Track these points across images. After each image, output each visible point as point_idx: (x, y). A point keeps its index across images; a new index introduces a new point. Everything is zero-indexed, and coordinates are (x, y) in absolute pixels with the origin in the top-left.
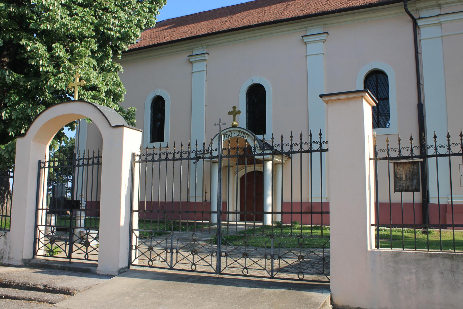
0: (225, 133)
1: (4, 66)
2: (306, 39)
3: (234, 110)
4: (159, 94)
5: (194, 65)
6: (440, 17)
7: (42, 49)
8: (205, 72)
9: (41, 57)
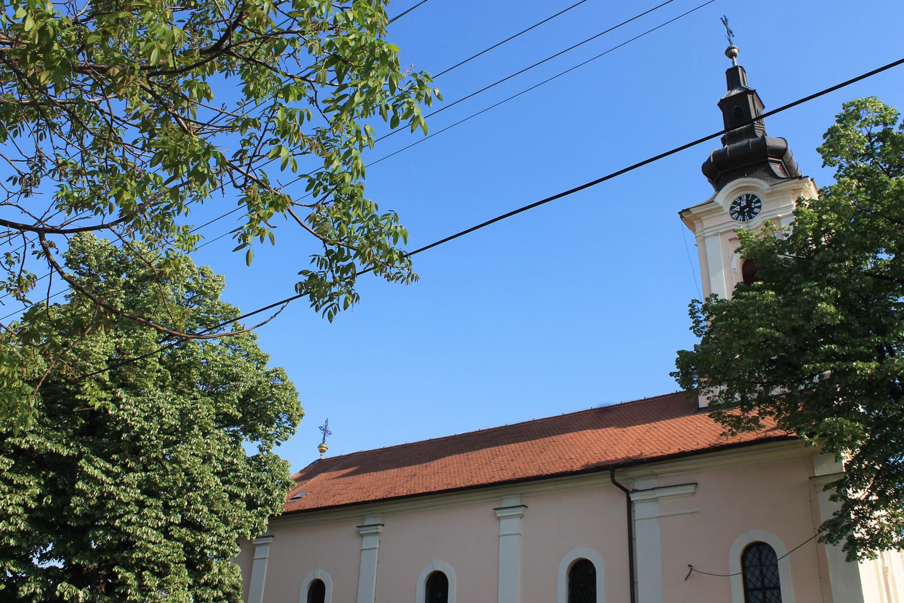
1: (100, 579)
2: (500, 514)
5: (365, 539)
6: (655, 491)
7: (131, 577)
8: (377, 550)
9: (129, 586)
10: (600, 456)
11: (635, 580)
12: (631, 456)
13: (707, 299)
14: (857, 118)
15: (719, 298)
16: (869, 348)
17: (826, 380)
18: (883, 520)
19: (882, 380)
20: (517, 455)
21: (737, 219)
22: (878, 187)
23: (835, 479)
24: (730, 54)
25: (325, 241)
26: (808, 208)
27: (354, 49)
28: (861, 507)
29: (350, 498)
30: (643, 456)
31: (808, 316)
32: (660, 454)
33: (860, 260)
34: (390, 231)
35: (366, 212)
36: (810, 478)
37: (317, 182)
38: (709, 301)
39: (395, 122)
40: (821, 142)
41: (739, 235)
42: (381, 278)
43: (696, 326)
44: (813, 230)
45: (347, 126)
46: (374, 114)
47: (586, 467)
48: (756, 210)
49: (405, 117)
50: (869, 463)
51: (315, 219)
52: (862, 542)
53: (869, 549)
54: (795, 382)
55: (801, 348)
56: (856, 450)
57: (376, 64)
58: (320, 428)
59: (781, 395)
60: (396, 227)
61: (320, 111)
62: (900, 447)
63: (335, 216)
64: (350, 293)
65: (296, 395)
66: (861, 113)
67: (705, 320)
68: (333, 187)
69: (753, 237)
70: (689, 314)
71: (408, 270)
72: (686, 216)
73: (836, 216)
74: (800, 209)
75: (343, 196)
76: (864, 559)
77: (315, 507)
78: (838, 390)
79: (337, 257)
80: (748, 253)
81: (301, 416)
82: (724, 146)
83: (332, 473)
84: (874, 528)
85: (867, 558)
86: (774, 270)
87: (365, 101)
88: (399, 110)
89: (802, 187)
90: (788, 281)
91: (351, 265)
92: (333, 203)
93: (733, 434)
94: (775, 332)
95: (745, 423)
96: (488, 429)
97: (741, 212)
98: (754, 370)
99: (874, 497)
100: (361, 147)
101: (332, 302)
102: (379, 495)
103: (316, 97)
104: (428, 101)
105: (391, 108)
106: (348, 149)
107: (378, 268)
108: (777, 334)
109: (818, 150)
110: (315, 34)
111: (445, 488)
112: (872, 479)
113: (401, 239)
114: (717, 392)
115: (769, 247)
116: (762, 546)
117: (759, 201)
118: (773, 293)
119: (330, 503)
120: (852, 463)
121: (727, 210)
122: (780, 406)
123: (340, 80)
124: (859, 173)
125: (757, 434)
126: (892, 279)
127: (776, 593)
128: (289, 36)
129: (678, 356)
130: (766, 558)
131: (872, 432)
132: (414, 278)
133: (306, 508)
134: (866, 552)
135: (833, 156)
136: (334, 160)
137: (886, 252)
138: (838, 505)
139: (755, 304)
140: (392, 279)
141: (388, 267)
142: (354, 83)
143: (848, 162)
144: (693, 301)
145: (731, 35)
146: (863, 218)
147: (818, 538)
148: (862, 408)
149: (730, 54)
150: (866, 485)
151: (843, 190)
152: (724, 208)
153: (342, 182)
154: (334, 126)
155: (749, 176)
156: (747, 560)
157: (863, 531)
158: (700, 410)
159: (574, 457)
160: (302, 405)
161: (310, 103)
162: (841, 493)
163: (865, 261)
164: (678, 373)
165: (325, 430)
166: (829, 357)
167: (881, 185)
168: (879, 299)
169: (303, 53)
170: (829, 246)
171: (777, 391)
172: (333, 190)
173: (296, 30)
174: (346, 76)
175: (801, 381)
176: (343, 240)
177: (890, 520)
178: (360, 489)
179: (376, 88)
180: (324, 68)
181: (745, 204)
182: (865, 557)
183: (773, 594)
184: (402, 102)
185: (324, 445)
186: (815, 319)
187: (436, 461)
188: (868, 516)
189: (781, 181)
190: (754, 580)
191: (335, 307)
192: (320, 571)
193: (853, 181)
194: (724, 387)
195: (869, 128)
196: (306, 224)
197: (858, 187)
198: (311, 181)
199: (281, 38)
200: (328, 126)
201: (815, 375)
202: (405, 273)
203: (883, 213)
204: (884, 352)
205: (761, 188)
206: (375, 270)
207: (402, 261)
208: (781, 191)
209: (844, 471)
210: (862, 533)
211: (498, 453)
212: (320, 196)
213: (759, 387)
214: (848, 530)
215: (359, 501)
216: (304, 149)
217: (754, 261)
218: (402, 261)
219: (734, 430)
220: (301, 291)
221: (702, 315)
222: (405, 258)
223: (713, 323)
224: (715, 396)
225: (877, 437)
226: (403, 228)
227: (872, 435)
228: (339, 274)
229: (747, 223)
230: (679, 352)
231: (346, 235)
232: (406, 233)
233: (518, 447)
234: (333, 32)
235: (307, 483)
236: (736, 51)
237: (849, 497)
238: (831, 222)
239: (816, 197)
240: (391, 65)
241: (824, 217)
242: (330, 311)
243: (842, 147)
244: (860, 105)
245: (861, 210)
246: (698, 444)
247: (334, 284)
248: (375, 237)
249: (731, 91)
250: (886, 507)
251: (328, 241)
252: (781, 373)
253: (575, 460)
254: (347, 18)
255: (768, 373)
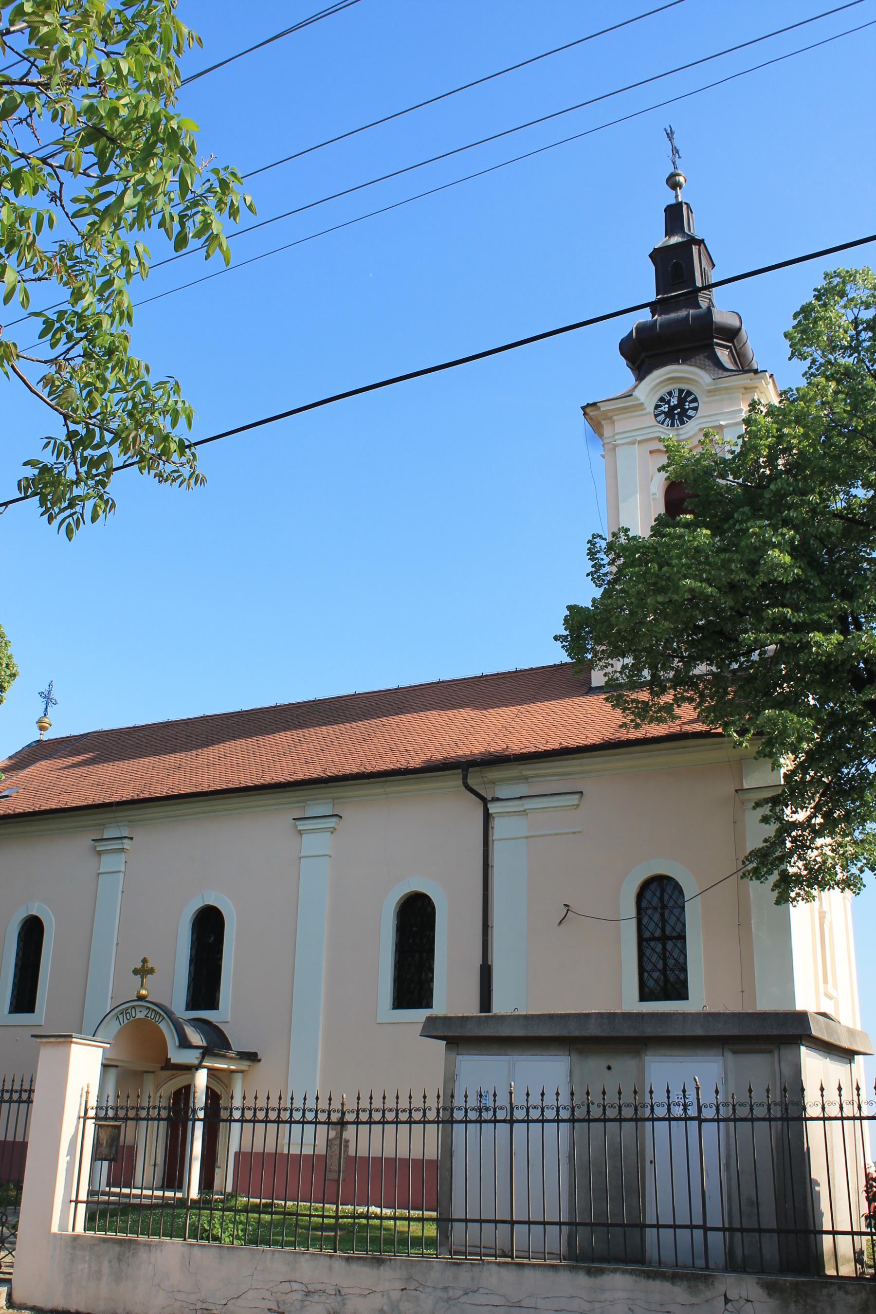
0: (123, 1009)
2: (302, 826)
3: (143, 966)
4: (34, 913)
5: (105, 858)
6: (524, 801)
8: (122, 875)
10: (449, 749)
11: (489, 924)
12: (492, 750)
13: (614, 535)
14: (842, 294)
15: (631, 534)
16: (830, 617)
17: (768, 658)
18: (827, 851)
19: (843, 663)
20: (329, 743)
21: (662, 423)
22: (860, 395)
23: (769, 794)
24: (673, 183)
25: (66, 417)
26: (764, 417)
27: (126, 121)
28: (800, 832)
29: (83, 798)
30: (510, 752)
31: (752, 567)
32: (533, 749)
33: (828, 495)
34: (167, 408)
35: (131, 376)
36: (736, 791)
37: (57, 325)
38: (617, 538)
39: (181, 242)
40: (790, 324)
41: (665, 446)
42: (148, 478)
43: (596, 572)
44: (769, 447)
45: (108, 242)
46: (149, 226)
47: (429, 763)
48: (690, 413)
49: (198, 235)
50: (815, 774)
51: (53, 382)
52: (798, 880)
53: (806, 888)
54: (727, 658)
55: (738, 612)
56: (800, 755)
57: (159, 148)
58: (41, 694)
59: (707, 675)
60: (176, 402)
61: (67, 214)
62: (857, 753)
63: (85, 379)
64: (101, 497)
65: (6, 644)
66: (848, 287)
67: (609, 564)
68: (82, 334)
69: (685, 452)
70: (588, 554)
71: (191, 467)
72: (591, 414)
73: (802, 430)
74: (754, 416)
75: (97, 350)
76: (798, 901)
77: (31, 810)
78: (784, 673)
79: (84, 443)
80: (676, 472)
81: (13, 675)
82: (653, 317)
83: (58, 761)
84: (815, 860)
85: (803, 899)
86: (710, 499)
87: (140, 205)
88: (189, 224)
89: (757, 385)
90: (729, 516)
91: (105, 457)
92: (81, 359)
93: (637, 726)
94: (707, 586)
95: (654, 712)
96: (290, 704)
97: (670, 414)
98: (673, 639)
99: (819, 820)
100: (129, 275)
101: (74, 510)
102: (127, 794)
103: (60, 192)
104: (234, 212)
105: (176, 219)
106: (107, 277)
107: (144, 461)
108: (710, 590)
109: (786, 335)
110: (67, 90)
111: (224, 787)
112: (818, 795)
113: (182, 420)
114: (618, 665)
115: (707, 467)
116: (665, 882)
117: (695, 400)
118: (709, 532)
119: (53, 805)
120: (793, 772)
121: (650, 408)
122: (703, 690)
123: (102, 169)
124: (837, 372)
125: (670, 727)
126: (867, 525)
127: (679, 944)
128: (25, 90)
129: (568, 613)
130: (670, 897)
131: (823, 732)
132: (199, 480)
133: (17, 812)
134: (802, 893)
135: (805, 345)
136: (86, 293)
137: (863, 486)
138: (771, 830)
139: (682, 546)
140: (166, 480)
141: (161, 462)
142: (124, 174)
143: (823, 356)
144: (594, 536)
145: (677, 155)
146: (838, 436)
147: (740, 873)
148: (813, 698)
149: (673, 183)
150: (810, 803)
151: (816, 395)
152: (646, 405)
153: (96, 328)
154: (86, 240)
155: (684, 362)
156: (644, 900)
157: (800, 864)
158: (591, 690)
159: (411, 749)
160: (15, 660)
161: (52, 200)
162: (775, 813)
163: (834, 497)
164: (566, 637)
165: (48, 698)
166: (779, 625)
167: (865, 393)
168: (848, 551)
169: (43, 121)
170: (788, 472)
171: (701, 669)
172: (82, 339)
173: (36, 81)
174: (112, 164)
175: (734, 657)
176: (95, 417)
177: (835, 850)
178: (98, 785)
179: (158, 186)
180: (79, 147)
181: (676, 403)
182: (800, 899)
183: (675, 945)
184: (194, 210)
185: (46, 720)
186: (762, 572)
187: (211, 748)
188: (808, 844)
189: (729, 373)
190: (652, 926)
191: (78, 517)
192: (37, 904)
193: (830, 383)
194: (629, 660)
195: (856, 311)
196: (39, 389)
197: (836, 393)
198: (49, 324)
199: (12, 92)
200: (79, 240)
201: (754, 650)
202: (186, 471)
203: (864, 433)
204: (849, 624)
205: (700, 381)
206: (140, 465)
207: (182, 454)
208: (726, 389)
209: (782, 783)
210: (798, 867)
211: (303, 739)
212: (61, 348)
213: (676, 663)
214: (782, 862)
215: (97, 803)
216: (40, 273)
217: (684, 485)
218: (182, 454)
219: (638, 721)
220: (26, 491)
221: (604, 557)
222: (187, 450)
223: (620, 570)
224: (616, 672)
225: (829, 739)
226: (187, 405)
227: (822, 737)
228: (85, 468)
229: (676, 429)
230: (569, 608)
231: (98, 410)
232: (191, 411)
233: (331, 732)
234: (94, 91)
235: (20, 775)
236: (681, 179)
237: (786, 819)
238: (794, 437)
239: (775, 401)
240: (183, 152)
241: (786, 431)
242: (69, 523)
243: (820, 334)
244: (849, 277)
245: (835, 425)
246: (587, 737)
247: (76, 483)
248: (144, 415)
249: (670, 237)
250: (832, 834)
251: (72, 417)
252: (709, 645)
253: (412, 753)
254: (117, 69)
255: (692, 644)
